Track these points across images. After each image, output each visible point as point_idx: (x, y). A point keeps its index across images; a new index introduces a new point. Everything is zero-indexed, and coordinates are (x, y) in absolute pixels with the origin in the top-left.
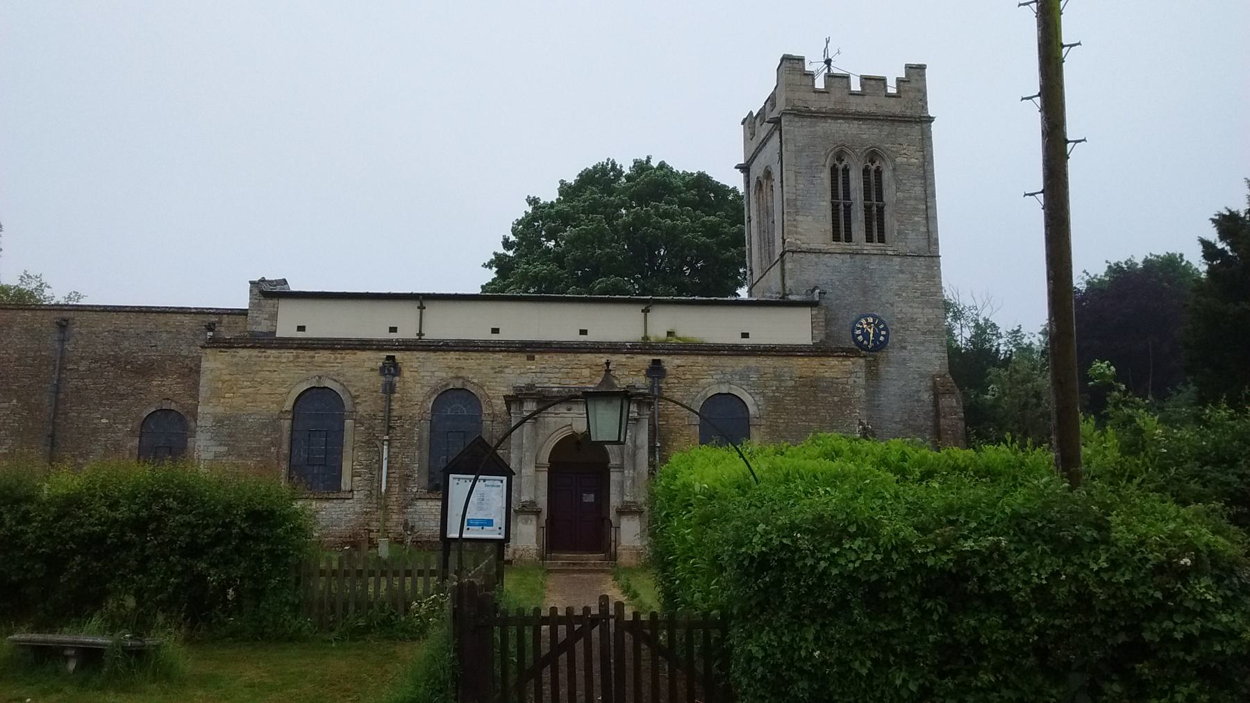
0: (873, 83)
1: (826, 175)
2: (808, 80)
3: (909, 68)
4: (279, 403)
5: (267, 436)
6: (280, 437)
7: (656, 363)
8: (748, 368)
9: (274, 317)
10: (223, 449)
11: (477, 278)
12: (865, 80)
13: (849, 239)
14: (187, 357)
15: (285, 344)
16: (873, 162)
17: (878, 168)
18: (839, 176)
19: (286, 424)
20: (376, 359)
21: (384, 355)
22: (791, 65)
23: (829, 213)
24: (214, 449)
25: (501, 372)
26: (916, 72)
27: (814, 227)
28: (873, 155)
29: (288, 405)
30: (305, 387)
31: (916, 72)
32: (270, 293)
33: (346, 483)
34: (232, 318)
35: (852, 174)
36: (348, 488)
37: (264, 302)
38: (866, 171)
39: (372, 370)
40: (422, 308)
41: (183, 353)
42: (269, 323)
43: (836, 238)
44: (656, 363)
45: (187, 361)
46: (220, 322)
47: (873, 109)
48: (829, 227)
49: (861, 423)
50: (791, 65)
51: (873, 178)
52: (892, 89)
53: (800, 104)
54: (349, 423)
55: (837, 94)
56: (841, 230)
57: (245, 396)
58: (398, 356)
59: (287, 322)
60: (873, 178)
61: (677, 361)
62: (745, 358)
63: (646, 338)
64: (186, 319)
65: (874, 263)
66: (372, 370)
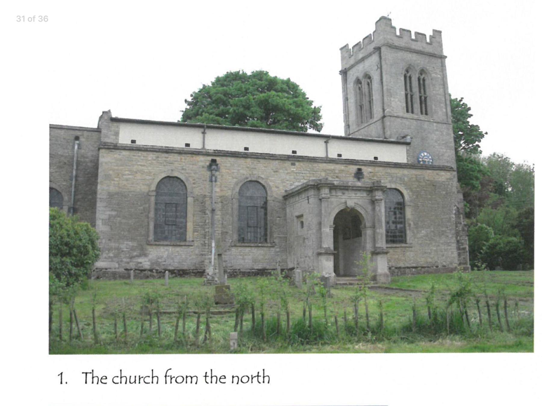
0: (420, 36)
1: (402, 78)
2: (393, 30)
3: (435, 31)
4: (149, 186)
5: (141, 206)
6: (149, 206)
7: (359, 170)
8: (404, 175)
9: (117, 134)
10: (114, 213)
11: (177, 117)
12: (417, 34)
13: (412, 112)
14: (62, 156)
15: (125, 148)
16: (421, 74)
17: (424, 78)
18: (407, 79)
19: (153, 199)
20: (205, 161)
21: (210, 158)
22: (384, 22)
23: (404, 97)
24: (108, 213)
25: (277, 171)
26: (437, 33)
27: (397, 104)
28: (422, 71)
29: (153, 187)
30: (163, 175)
31: (437, 33)
32: (110, 120)
33: (190, 235)
34: (89, 133)
35: (413, 79)
36: (191, 239)
37: (110, 124)
38: (419, 79)
39: (203, 167)
40: (204, 133)
41: (59, 153)
42: (114, 137)
43: (407, 111)
44: (359, 170)
45: (62, 159)
46: (83, 135)
47: (421, 49)
48: (405, 105)
49: (455, 206)
50: (384, 22)
51: (421, 82)
52: (428, 40)
53: (390, 41)
54: (190, 200)
55: (406, 39)
56: (409, 108)
57: (127, 180)
58: (218, 159)
59: (126, 135)
60: (421, 82)
61: (370, 169)
62: (401, 169)
63: (327, 157)
64: (62, 132)
65: (426, 125)
66: (203, 167)
